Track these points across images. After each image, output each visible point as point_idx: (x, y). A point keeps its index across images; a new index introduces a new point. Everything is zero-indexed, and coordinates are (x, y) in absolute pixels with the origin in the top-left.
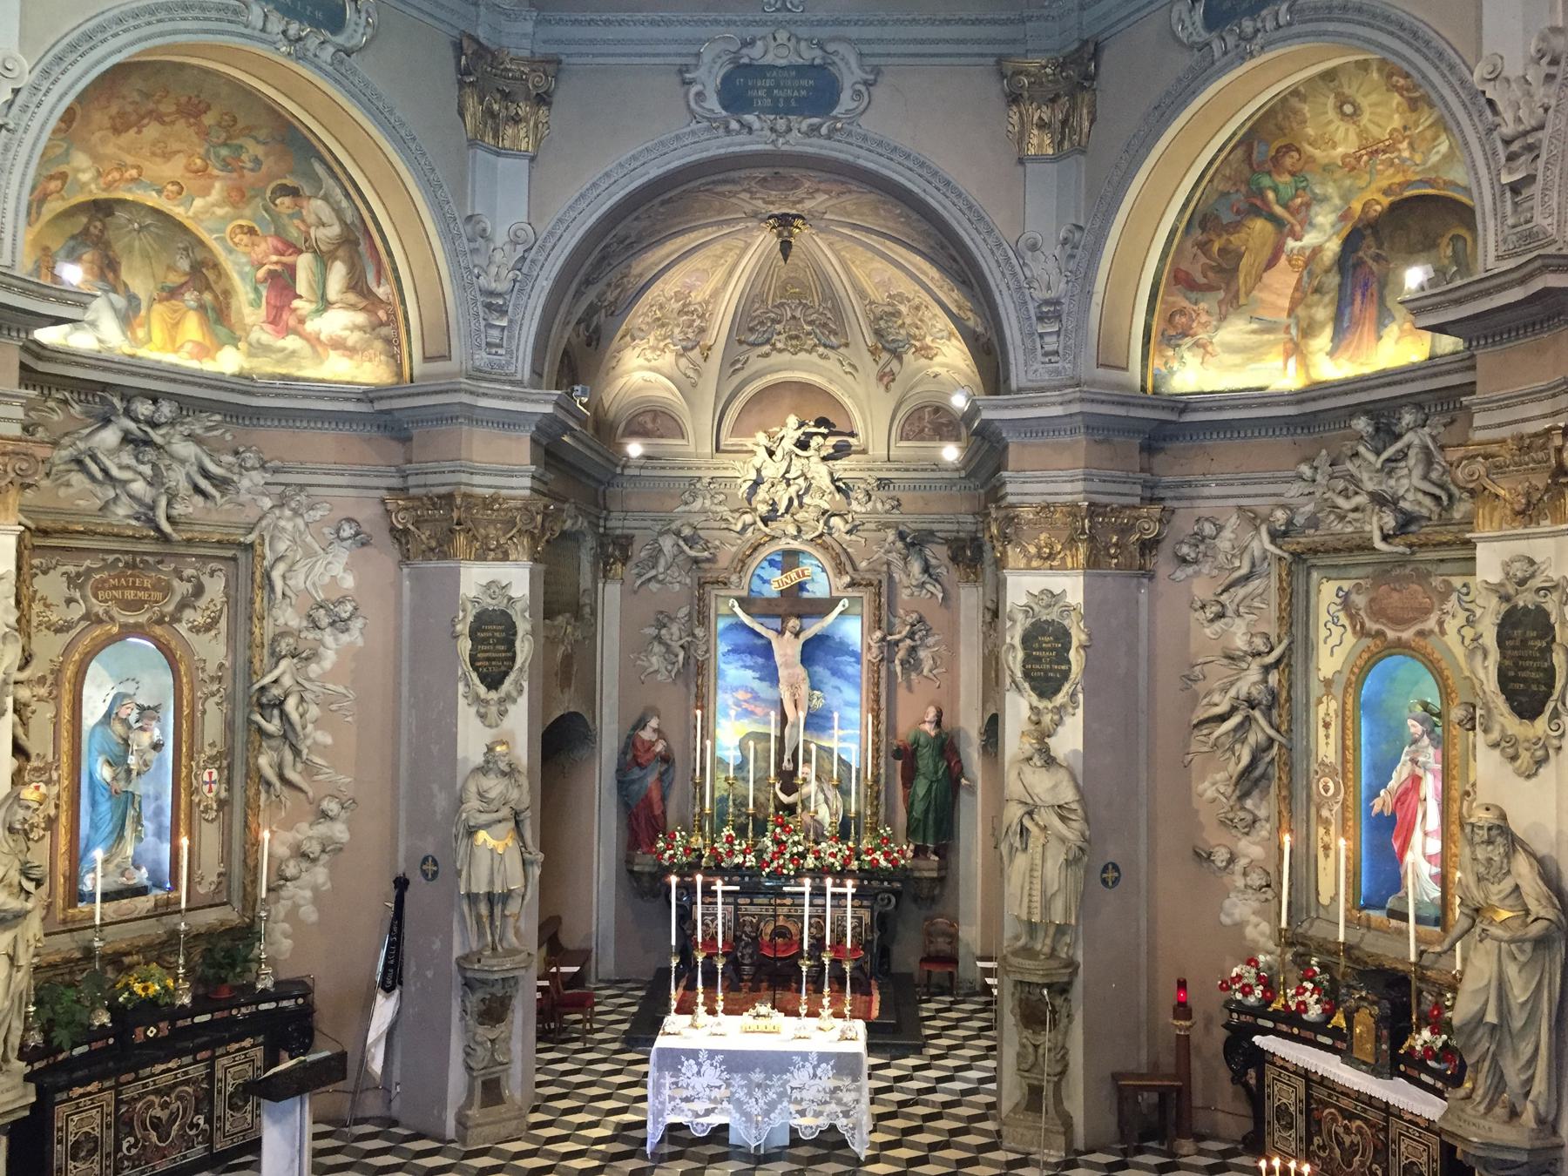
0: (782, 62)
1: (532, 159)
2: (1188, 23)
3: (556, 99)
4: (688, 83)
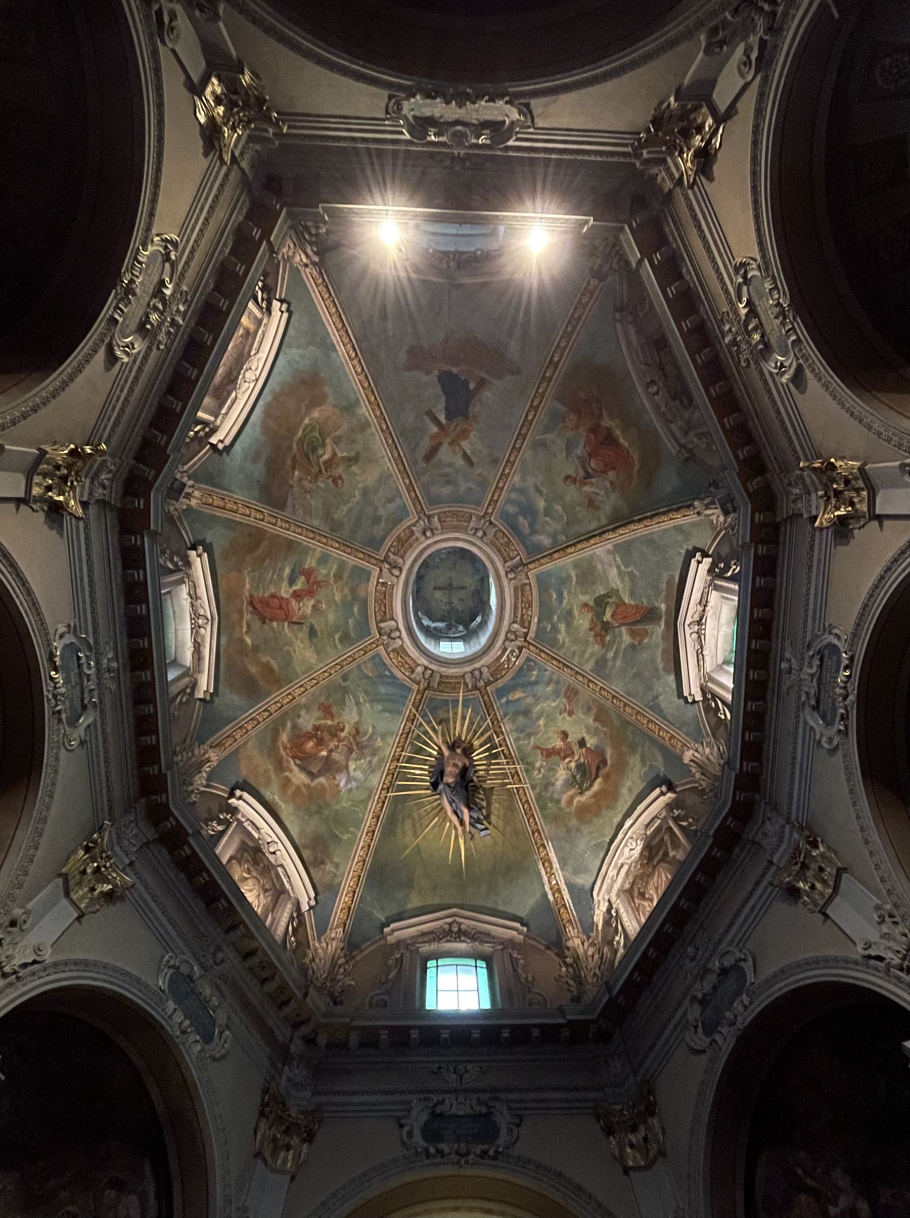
0: (461, 1113)
2: (697, 1040)
4: (401, 1126)
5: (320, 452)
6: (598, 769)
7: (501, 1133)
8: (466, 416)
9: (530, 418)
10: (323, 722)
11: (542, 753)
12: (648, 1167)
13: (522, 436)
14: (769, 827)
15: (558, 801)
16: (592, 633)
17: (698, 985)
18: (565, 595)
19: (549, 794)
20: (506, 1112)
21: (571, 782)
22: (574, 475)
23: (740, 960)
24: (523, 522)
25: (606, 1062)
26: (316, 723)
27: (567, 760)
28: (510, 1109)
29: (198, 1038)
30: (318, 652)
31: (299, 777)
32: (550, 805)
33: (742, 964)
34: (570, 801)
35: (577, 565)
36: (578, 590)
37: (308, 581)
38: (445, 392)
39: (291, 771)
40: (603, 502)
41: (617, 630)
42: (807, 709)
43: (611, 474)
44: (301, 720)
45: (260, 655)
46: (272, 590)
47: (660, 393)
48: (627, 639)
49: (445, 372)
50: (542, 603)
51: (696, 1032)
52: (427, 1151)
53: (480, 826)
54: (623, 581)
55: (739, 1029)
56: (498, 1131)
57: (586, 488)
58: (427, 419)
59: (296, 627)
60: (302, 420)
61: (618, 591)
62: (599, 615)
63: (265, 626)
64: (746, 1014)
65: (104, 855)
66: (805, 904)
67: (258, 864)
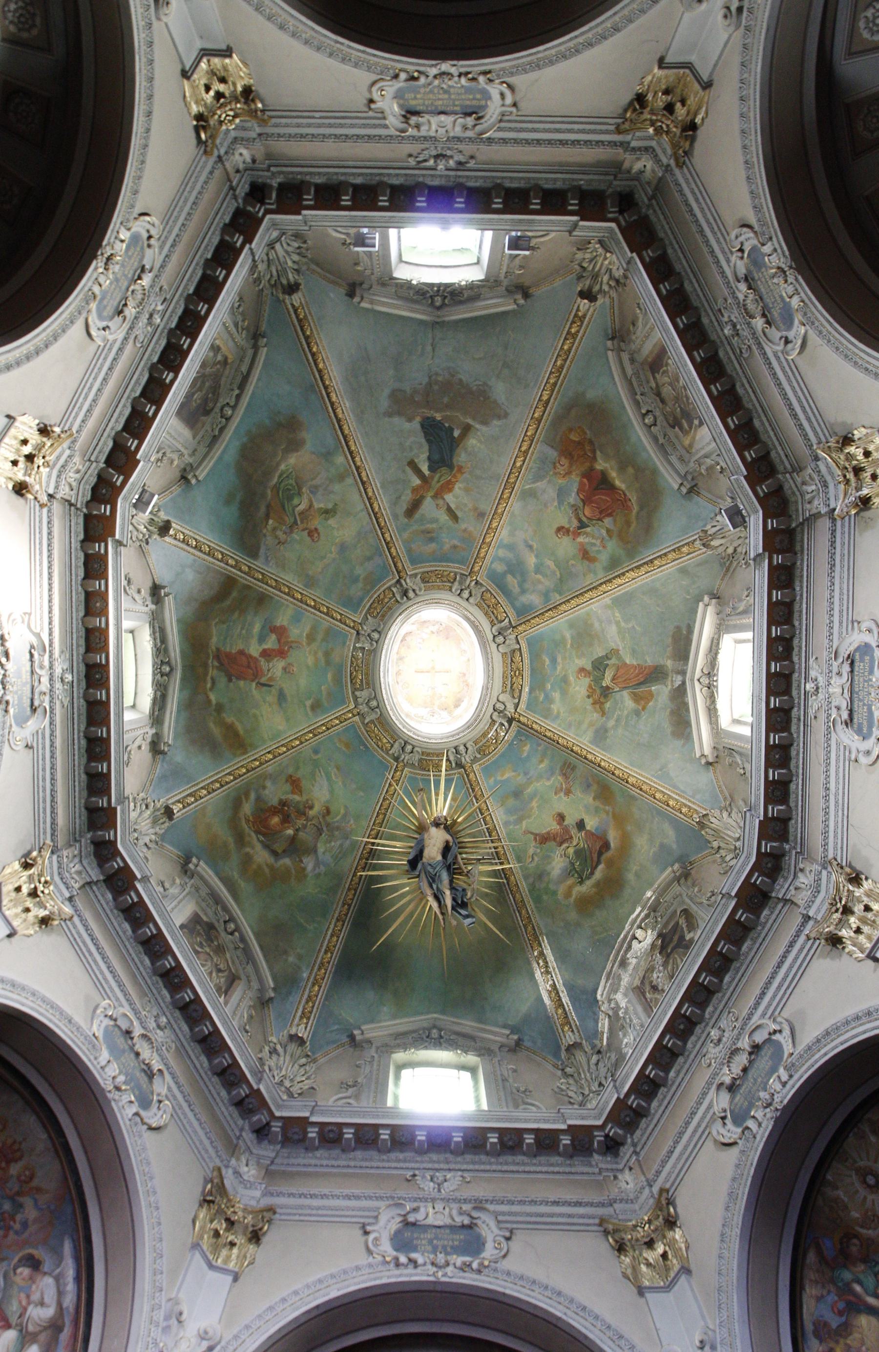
1: (236, 1279)
3: (265, 1240)
4: (366, 1233)
5: (296, 501)
6: (600, 854)
7: (487, 1245)
8: (451, 467)
9: (518, 464)
10: (290, 796)
11: (535, 839)
12: (668, 1288)
13: (509, 486)
14: (803, 880)
15: (555, 893)
16: (591, 700)
17: (726, 1070)
18: (559, 660)
19: (543, 885)
20: (492, 1224)
21: (570, 871)
22: (567, 526)
23: (775, 1032)
24: (512, 581)
25: (615, 1177)
26: (283, 797)
27: (565, 845)
28: (499, 1222)
29: (133, 1098)
30: (288, 720)
31: (261, 856)
32: (545, 897)
33: (777, 1037)
34: (568, 895)
35: (571, 625)
36: (574, 653)
37: (279, 640)
38: (428, 441)
39: (253, 848)
40: (599, 552)
41: (618, 696)
42: (840, 727)
43: (608, 521)
44: (267, 792)
45: (224, 715)
46: (241, 646)
47: (658, 422)
48: (629, 703)
49: (428, 418)
50: (533, 671)
51: (724, 1124)
52: (397, 1259)
53: (463, 912)
54: (623, 639)
55: (777, 1110)
56: (484, 1244)
57: (580, 539)
58: (409, 470)
59: (265, 688)
60: (278, 464)
61: (618, 650)
62: (598, 680)
63: (231, 684)
64: (785, 1091)
65: (43, 879)
66: (850, 954)
67: (212, 942)
